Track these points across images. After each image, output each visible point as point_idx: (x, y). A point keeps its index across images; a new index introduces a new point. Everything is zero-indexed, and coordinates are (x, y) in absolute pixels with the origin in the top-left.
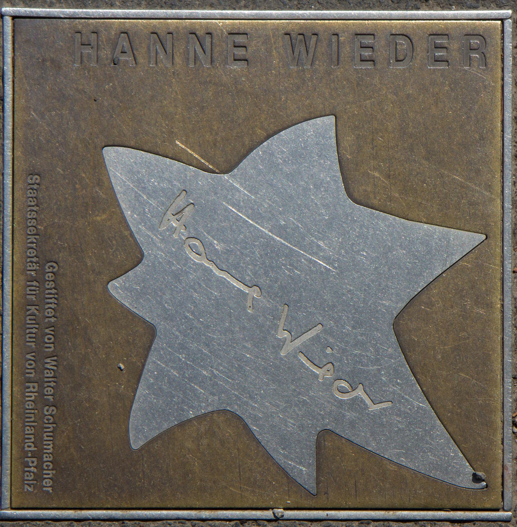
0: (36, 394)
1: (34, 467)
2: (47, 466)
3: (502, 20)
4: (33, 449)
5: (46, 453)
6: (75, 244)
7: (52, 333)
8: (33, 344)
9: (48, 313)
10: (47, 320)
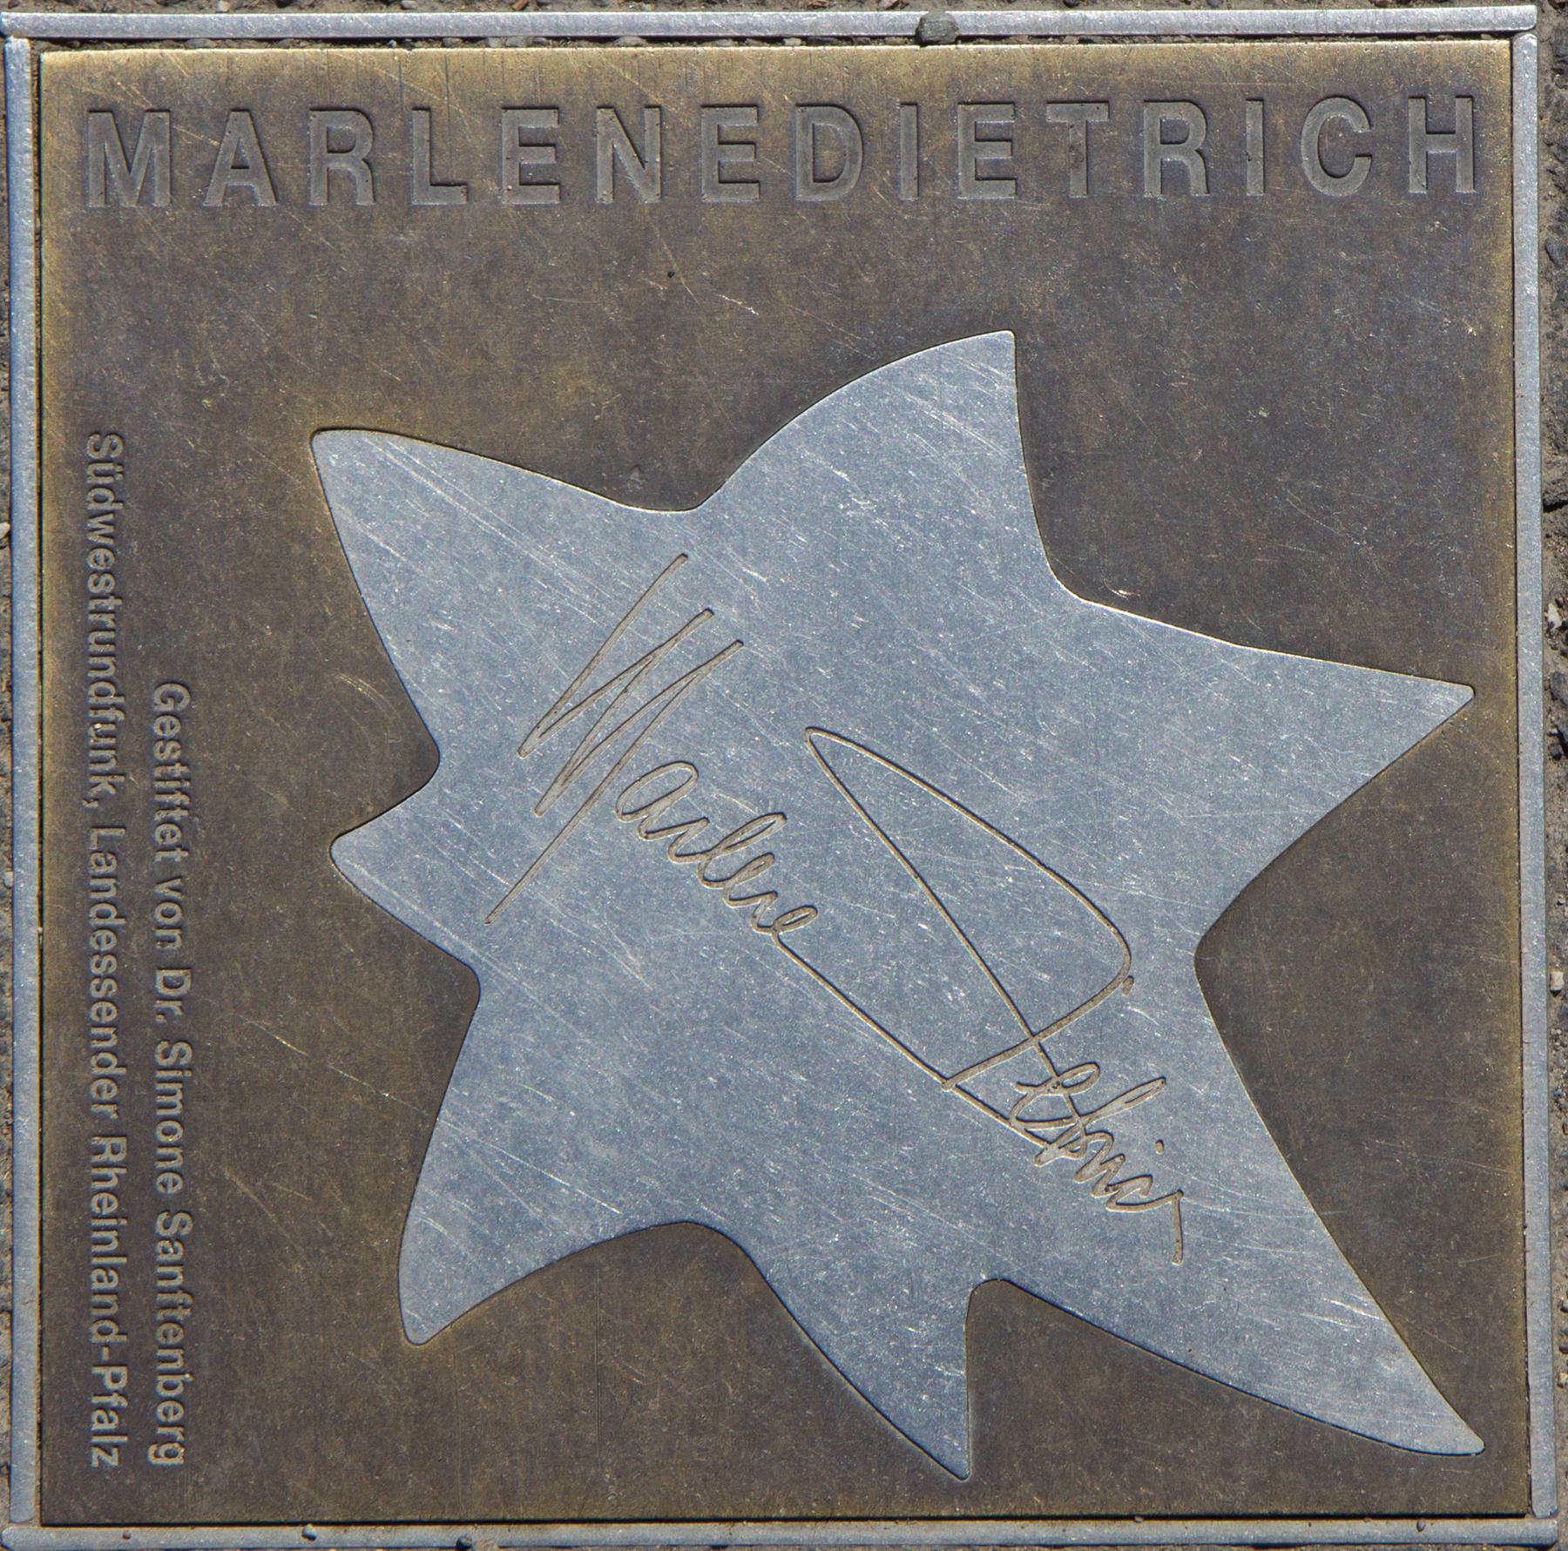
0: (123, 1171)
1: (122, 1394)
6: (233, 699)
7: (175, 895)
8: (110, 1109)
10: (160, 856)
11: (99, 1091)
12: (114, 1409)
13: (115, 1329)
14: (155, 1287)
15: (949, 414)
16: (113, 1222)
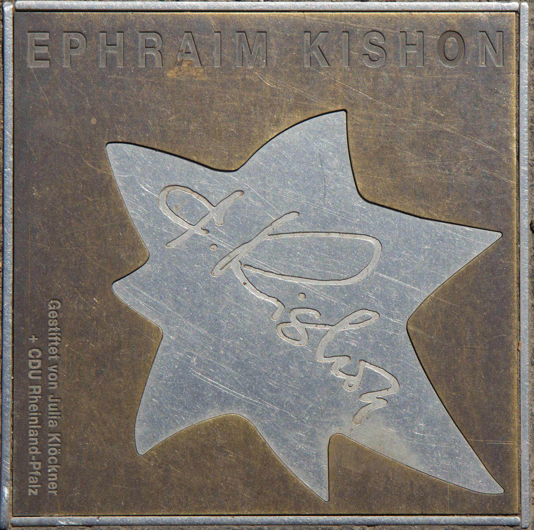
0: (40, 397)
1: (39, 471)
2: (51, 460)
4: (36, 452)
6: (77, 244)
7: (56, 371)
9: (51, 351)
11: (32, 408)
12: (36, 476)
13: (37, 449)
14: (48, 340)
15: (319, 143)
16: (37, 414)
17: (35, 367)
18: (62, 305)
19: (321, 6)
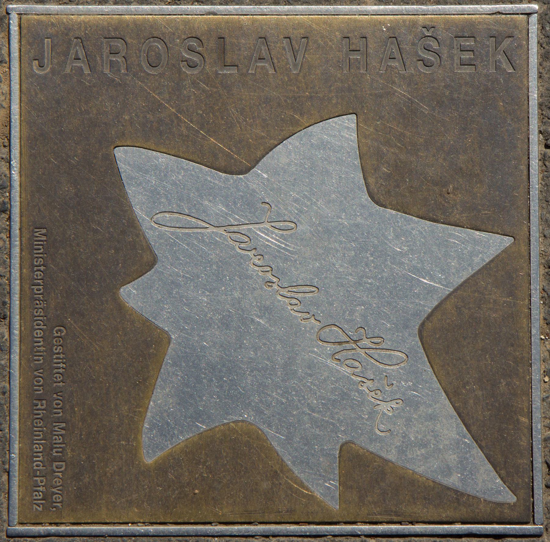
0: (44, 412)
3: (529, 14)
5: (55, 435)
6: (85, 245)
7: (59, 492)
10: (55, 384)
17: (39, 292)
18: (66, 330)
19: (518, 9)
